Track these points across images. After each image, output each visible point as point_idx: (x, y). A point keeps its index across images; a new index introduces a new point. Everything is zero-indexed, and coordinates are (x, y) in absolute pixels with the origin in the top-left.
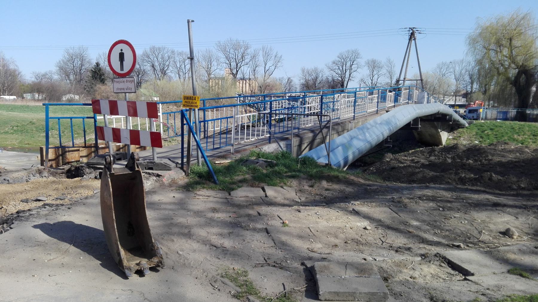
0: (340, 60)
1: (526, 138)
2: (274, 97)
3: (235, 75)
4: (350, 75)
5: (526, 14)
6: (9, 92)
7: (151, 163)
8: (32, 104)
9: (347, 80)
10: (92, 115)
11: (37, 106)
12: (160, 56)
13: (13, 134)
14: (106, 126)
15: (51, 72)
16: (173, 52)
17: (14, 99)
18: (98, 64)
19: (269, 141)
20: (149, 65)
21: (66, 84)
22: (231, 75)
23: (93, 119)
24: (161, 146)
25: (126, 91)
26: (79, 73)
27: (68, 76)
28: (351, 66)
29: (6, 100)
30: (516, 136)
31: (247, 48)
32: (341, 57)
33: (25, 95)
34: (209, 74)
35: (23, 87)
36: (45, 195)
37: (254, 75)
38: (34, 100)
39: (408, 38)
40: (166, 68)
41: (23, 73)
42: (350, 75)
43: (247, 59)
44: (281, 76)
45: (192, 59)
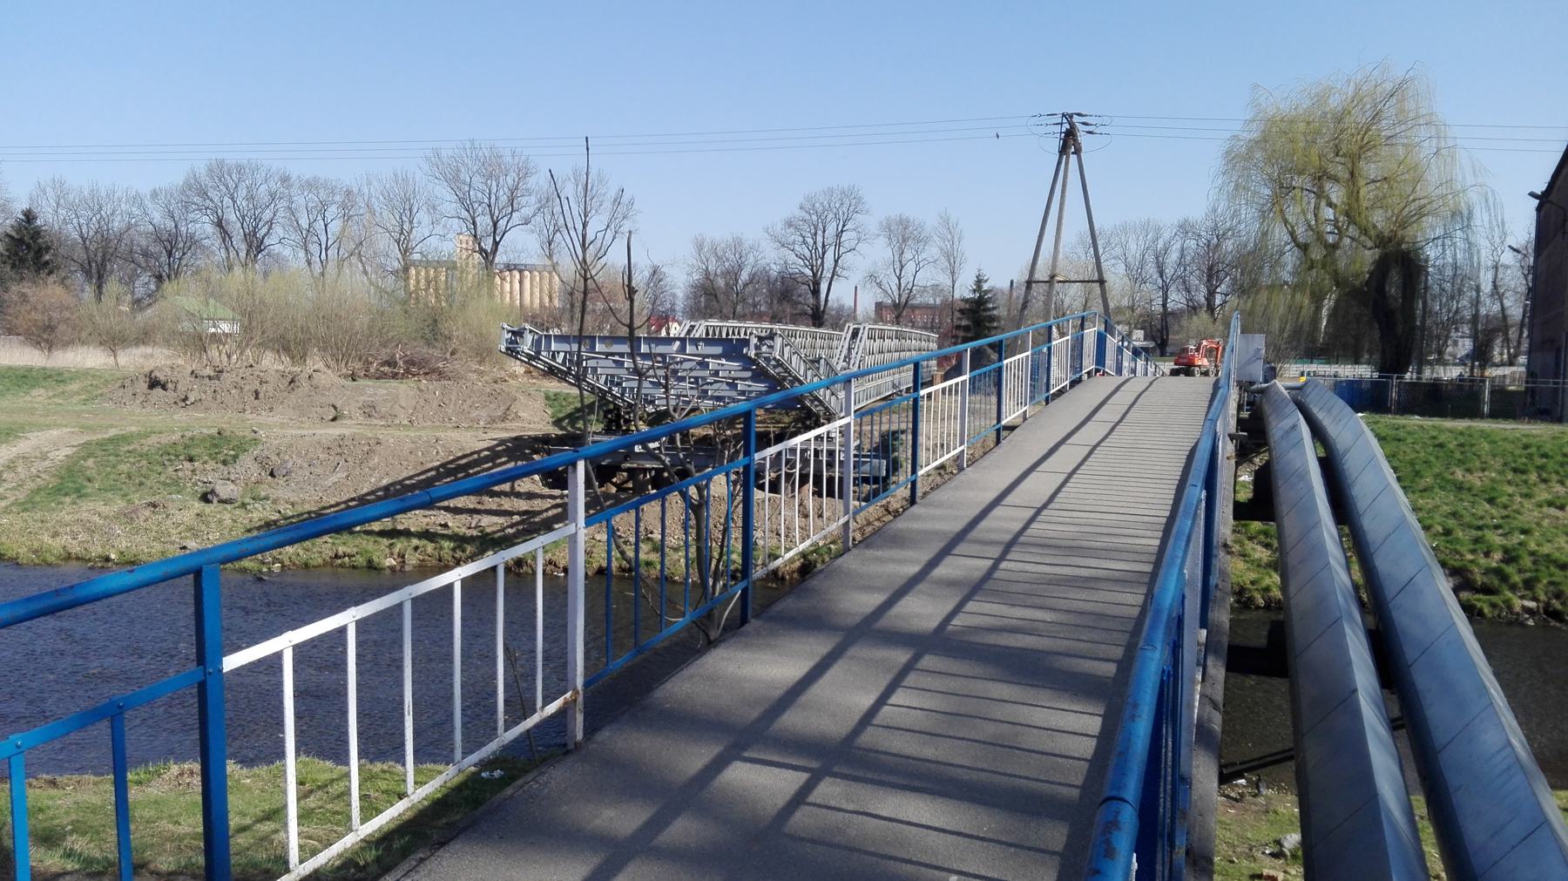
1: (1493, 480)
3: (488, 256)
4: (836, 261)
5: (1404, 81)
12: (242, 192)
16: (285, 180)
18: (29, 216)
20: (206, 219)
22: (477, 255)
28: (839, 235)
30: (1459, 474)
31: (524, 173)
32: (809, 207)
34: (405, 252)
37: (550, 257)
39: (1056, 144)
40: (264, 230)
42: (836, 261)
43: (528, 205)
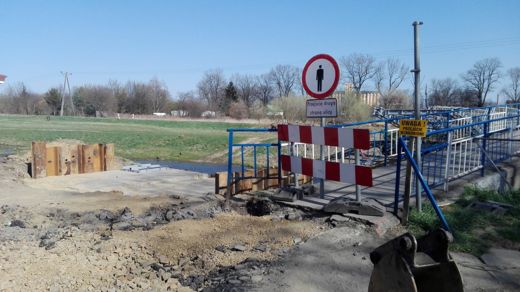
0: (477, 69)
2: (404, 111)
4: (489, 85)
6: (160, 109)
7: (354, 204)
8: (179, 120)
9: (485, 90)
10: (276, 142)
11: (183, 122)
13: (165, 147)
14: (292, 155)
15: (192, 92)
17: (164, 116)
18: (231, 84)
19: (482, 173)
21: (205, 102)
23: (277, 147)
24: (370, 185)
25: (323, 115)
26: (215, 92)
27: (206, 95)
29: (158, 117)
31: (371, 61)
33: (172, 112)
35: (171, 105)
36: (241, 242)
38: (180, 116)
41: (171, 93)
43: (372, 71)
44: (406, 88)
45: (417, 72)
